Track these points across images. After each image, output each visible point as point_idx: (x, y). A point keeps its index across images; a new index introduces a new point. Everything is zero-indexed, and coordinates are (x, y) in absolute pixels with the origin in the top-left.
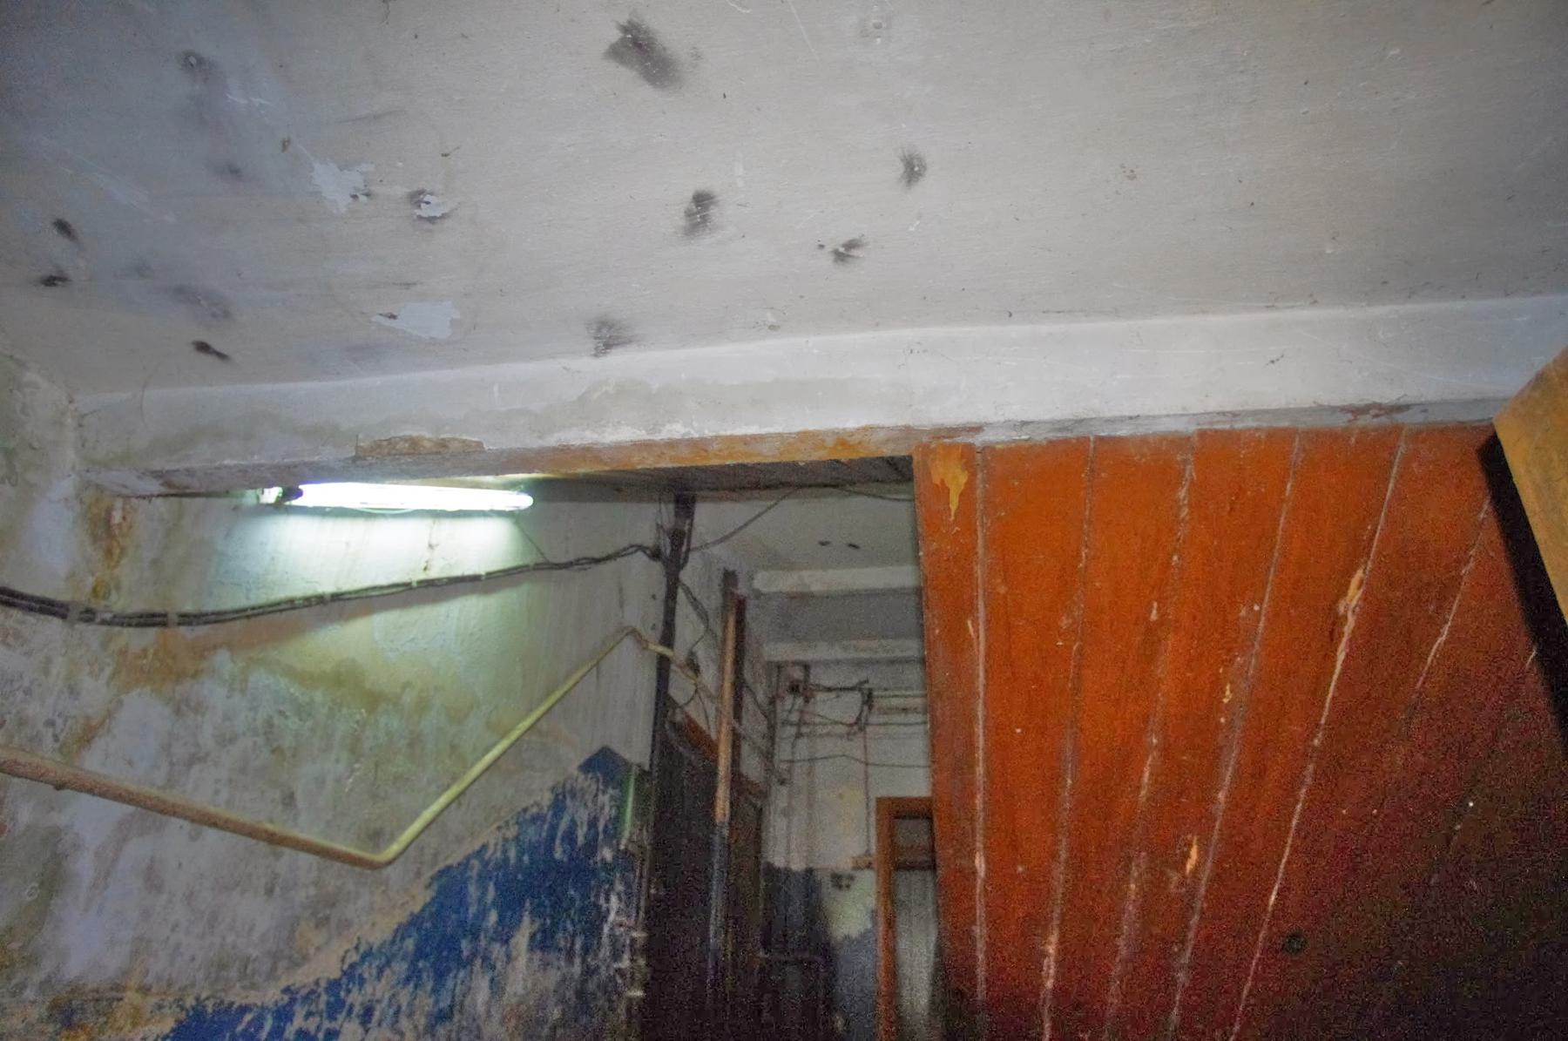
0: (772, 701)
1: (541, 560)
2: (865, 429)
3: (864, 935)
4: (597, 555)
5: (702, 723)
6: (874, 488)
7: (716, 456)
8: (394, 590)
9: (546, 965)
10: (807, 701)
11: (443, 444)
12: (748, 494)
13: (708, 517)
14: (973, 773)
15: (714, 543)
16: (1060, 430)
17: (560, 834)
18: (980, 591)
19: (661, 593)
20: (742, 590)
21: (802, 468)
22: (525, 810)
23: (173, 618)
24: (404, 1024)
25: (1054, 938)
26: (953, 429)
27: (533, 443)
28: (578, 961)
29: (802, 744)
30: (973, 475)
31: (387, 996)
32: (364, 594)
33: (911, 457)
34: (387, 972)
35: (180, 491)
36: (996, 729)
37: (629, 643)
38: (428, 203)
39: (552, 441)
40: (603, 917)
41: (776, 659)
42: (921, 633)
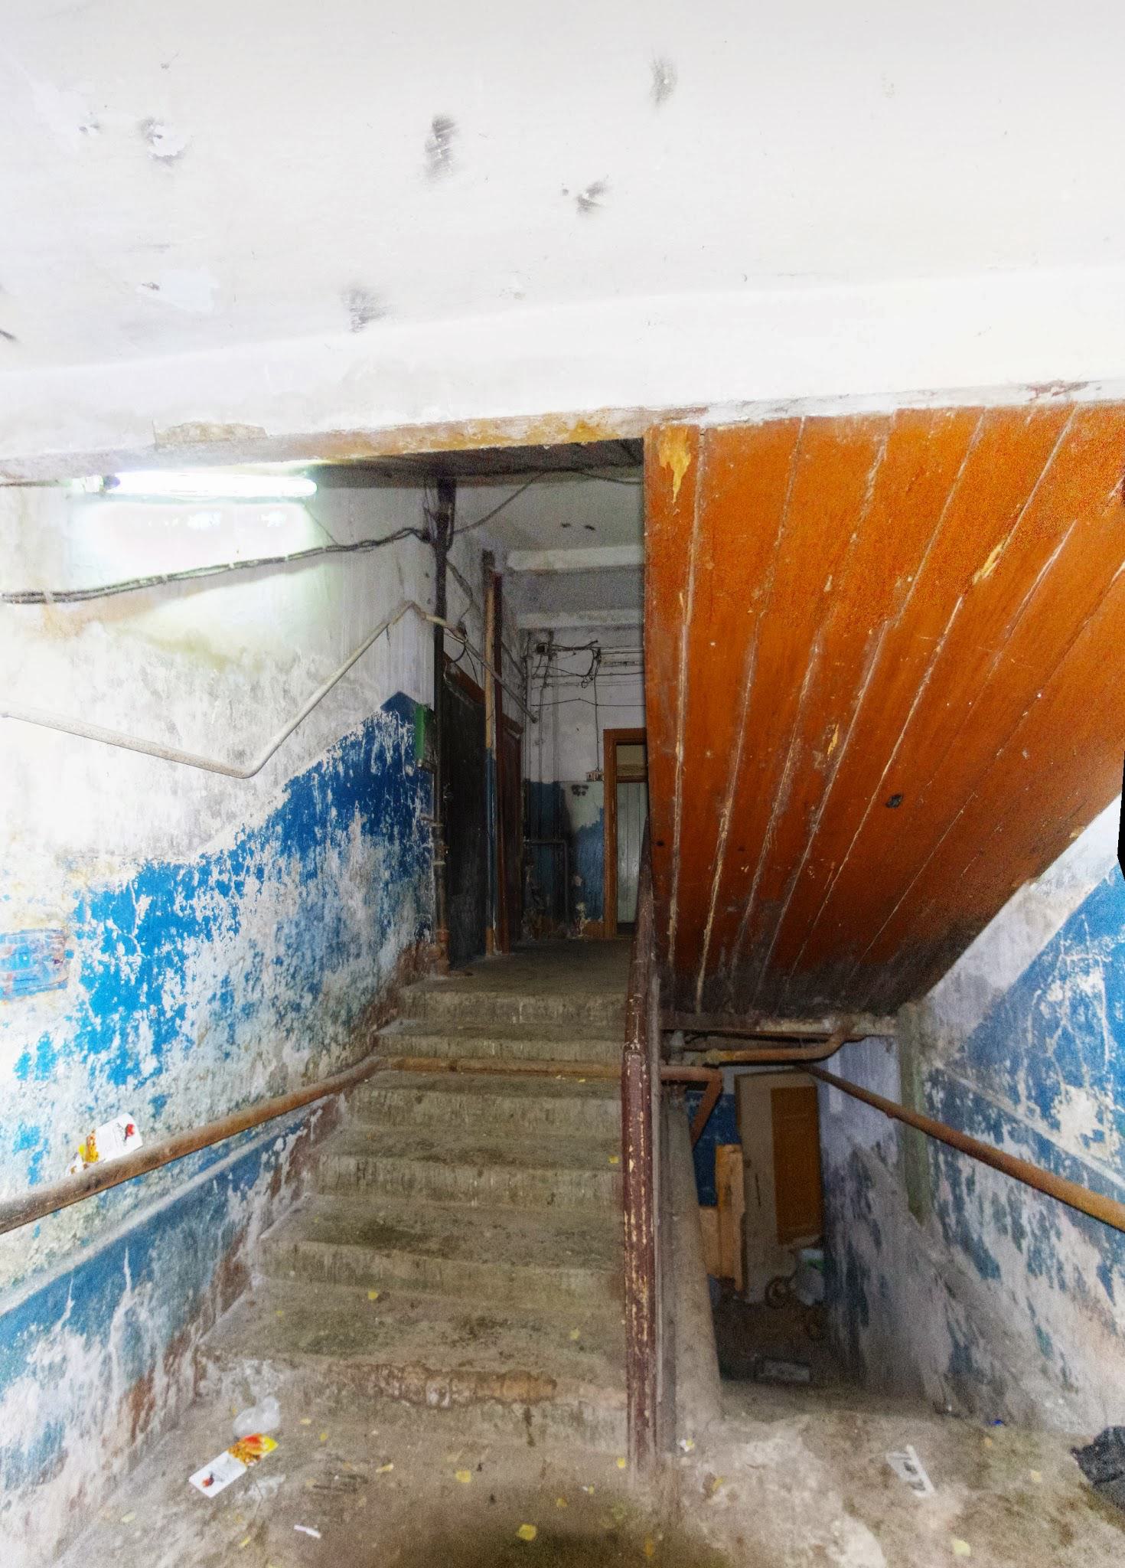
0: (524, 659)
1: (331, 543)
2: (603, 411)
3: (595, 825)
4: (377, 538)
5: (472, 676)
6: (610, 471)
7: (472, 441)
8: (217, 571)
9: (375, 845)
10: (550, 659)
11: (230, 430)
12: (500, 478)
13: (468, 500)
14: (677, 679)
15: (474, 526)
16: (776, 410)
17: (373, 756)
18: (692, 568)
19: (433, 573)
20: (498, 568)
21: (547, 451)
22: (346, 738)
23: (49, 596)
24: (286, 879)
25: (729, 803)
26: (681, 410)
27: (311, 429)
28: (397, 842)
29: (549, 691)
30: (695, 457)
31: (271, 861)
32: (191, 575)
33: (642, 440)
34: (267, 846)
35: (18, 481)
36: (696, 644)
37: (410, 615)
38: (160, 137)
39: (325, 426)
40: (410, 813)
41: (527, 627)
42: (642, 604)
